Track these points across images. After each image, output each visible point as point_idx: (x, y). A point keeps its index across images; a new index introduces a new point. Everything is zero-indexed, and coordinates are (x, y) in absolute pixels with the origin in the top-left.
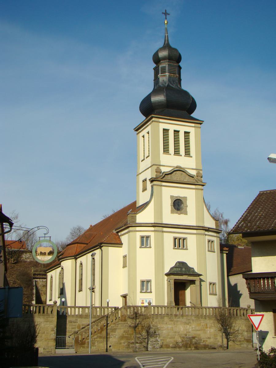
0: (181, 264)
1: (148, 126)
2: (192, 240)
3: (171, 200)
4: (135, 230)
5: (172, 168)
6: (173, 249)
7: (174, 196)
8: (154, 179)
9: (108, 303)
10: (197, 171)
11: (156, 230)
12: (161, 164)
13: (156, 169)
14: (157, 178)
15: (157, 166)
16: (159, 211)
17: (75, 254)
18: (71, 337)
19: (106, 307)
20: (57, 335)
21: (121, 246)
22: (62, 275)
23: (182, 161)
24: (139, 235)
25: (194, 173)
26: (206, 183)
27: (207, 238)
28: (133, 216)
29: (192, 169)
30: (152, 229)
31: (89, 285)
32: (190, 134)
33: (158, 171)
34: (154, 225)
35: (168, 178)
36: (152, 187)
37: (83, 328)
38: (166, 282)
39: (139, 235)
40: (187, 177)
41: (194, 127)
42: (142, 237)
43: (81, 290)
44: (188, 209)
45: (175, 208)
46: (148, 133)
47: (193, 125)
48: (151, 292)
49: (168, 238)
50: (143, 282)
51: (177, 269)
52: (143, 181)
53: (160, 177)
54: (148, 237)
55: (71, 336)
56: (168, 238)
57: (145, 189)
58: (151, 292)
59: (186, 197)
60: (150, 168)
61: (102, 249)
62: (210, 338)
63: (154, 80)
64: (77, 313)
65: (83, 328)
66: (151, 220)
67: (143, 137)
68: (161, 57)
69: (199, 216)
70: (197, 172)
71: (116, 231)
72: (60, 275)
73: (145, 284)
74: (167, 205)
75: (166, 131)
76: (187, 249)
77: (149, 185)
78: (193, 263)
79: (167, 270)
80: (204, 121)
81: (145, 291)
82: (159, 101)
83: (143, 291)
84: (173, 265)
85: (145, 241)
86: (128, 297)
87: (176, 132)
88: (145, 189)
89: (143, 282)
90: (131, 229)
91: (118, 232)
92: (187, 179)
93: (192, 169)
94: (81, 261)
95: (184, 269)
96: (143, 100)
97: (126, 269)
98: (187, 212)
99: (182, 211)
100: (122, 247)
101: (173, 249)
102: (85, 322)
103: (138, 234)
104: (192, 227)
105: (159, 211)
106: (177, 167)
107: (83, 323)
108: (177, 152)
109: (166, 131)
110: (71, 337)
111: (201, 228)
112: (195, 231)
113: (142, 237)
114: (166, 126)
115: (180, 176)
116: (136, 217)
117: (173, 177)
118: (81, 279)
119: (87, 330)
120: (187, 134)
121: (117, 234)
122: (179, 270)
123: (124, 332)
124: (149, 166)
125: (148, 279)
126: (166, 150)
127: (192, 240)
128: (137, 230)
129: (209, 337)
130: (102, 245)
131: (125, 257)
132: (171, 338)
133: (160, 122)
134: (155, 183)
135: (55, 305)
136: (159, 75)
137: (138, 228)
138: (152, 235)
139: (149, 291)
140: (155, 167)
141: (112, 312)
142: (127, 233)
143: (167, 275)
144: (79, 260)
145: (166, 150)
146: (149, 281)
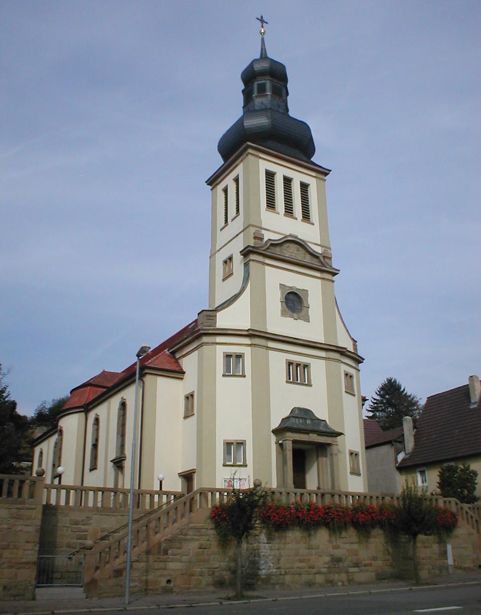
0: (303, 413)
1: (237, 166)
2: (318, 368)
3: (282, 293)
4: (214, 341)
5: (282, 236)
6: (287, 382)
7: (286, 285)
8: (251, 249)
9: (161, 482)
10: (324, 249)
11: (254, 343)
12: (263, 226)
13: (254, 233)
14: (258, 248)
15: (253, 228)
16: (259, 308)
17: (86, 401)
18: (74, 558)
19: (157, 492)
20: (40, 552)
21: (182, 377)
22: (58, 447)
23: (295, 227)
24: (220, 351)
25: (319, 250)
26: (339, 271)
27: (344, 368)
28: (209, 316)
29: (315, 244)
30: (247, 341)
31: (113, 455)
32: (185, 375)
33: (258, 238)
34: (251, 334)
35: (277, 251)
36: (245, 266)
37: (103, 539)
38: (274, 447)
39: (220, 351)
40: (308, 257)
41: (316, 177)
42: (228, 356)
43: (93, 468)
44: (311, 312)
45: (288, 307)
46: (237, 180)
47: (314, 174)
48: (245, 465)
49: (277, 361)
50: (228, 444)
51: (297, 420)
52: (225, 262)
53: (262, 247)
54: (239, 356)
55: (74, 555)
56: (277, 361)
57: (227, 276)
58: (245, 465)
59: (307, 291)
60: (242, 233)
61: (144, 379)
62: (377, 559)
63: (243, 107)
64: (91, 504)
65: (103, 539)
66: (245, 324)
67: (225, 191)
68: (258, 69)
69: (329, 327)
70: (323, 251)
71: (170, 351)
72: (55, 447)
73: (233, 447)
74: (274, 301)
75: (270, 176)
76: (309, 385)
77: (238, 259)
78: (321, 412)
79: (275, 424)
80: (330, 171)
81: (231, 463)
82: (259, 125)
83: (228, 463)
84: (287, 413)
85: (233, 361)
86: (195, 476)
87: (287, 181)
88: (227, 276)
89: (228, 444)
90: (205, 339)
91: (173, 353)
92: (308, 259)
93: (315, 244)
94: (96, 414)
95: (309, 422)
96: (221, 138)
97: (193, 420)
98: (309, 316)
99: (302, 314)
100: (182, 379)
101: (287, 382)
102: (110, 523)
103: (219, 351)
104: (319, 345)
105: (259, 308)
106: (290, 236)
107: (105, 526)
108: (289, 211)
109: (270, 176)
110: (74, 558)
111: (334, 348)
112: (323, 354)
113: (228, 356)
114: (272, 167)
115: (296, 252)
116: (216, 316)
117: (285, 251)
118: (95, 446)
119: (117, 542)
120: (304, 187)
121: (172, 356)
122: (301, 421)
123: (200, 548)
124: (240, 231)
125: (239, 438)
126: (271, 204)
127: (318, 368)
128: (217, 341)
129: (374, 557)
130: (144, 372)
131: (189, 397)
132: (301, 561)
133: (260, 158)
134: (252, 257)
135: (40, 478)
136: (254, 96)
137: (219, 339)
138: (247, 352)
139: (242, 463)
140: (252, 230)
141: (168, 502)
142: (196, 349)
143: (275, 432)
144: (92, 416)
145: (271, 204)
146: (241, 444)
